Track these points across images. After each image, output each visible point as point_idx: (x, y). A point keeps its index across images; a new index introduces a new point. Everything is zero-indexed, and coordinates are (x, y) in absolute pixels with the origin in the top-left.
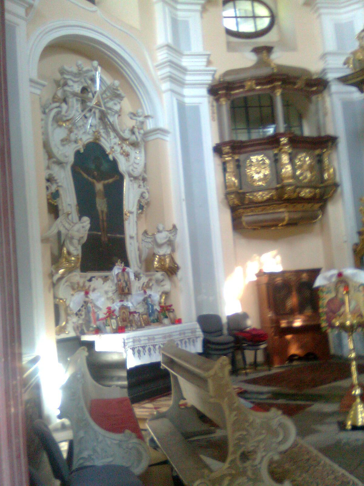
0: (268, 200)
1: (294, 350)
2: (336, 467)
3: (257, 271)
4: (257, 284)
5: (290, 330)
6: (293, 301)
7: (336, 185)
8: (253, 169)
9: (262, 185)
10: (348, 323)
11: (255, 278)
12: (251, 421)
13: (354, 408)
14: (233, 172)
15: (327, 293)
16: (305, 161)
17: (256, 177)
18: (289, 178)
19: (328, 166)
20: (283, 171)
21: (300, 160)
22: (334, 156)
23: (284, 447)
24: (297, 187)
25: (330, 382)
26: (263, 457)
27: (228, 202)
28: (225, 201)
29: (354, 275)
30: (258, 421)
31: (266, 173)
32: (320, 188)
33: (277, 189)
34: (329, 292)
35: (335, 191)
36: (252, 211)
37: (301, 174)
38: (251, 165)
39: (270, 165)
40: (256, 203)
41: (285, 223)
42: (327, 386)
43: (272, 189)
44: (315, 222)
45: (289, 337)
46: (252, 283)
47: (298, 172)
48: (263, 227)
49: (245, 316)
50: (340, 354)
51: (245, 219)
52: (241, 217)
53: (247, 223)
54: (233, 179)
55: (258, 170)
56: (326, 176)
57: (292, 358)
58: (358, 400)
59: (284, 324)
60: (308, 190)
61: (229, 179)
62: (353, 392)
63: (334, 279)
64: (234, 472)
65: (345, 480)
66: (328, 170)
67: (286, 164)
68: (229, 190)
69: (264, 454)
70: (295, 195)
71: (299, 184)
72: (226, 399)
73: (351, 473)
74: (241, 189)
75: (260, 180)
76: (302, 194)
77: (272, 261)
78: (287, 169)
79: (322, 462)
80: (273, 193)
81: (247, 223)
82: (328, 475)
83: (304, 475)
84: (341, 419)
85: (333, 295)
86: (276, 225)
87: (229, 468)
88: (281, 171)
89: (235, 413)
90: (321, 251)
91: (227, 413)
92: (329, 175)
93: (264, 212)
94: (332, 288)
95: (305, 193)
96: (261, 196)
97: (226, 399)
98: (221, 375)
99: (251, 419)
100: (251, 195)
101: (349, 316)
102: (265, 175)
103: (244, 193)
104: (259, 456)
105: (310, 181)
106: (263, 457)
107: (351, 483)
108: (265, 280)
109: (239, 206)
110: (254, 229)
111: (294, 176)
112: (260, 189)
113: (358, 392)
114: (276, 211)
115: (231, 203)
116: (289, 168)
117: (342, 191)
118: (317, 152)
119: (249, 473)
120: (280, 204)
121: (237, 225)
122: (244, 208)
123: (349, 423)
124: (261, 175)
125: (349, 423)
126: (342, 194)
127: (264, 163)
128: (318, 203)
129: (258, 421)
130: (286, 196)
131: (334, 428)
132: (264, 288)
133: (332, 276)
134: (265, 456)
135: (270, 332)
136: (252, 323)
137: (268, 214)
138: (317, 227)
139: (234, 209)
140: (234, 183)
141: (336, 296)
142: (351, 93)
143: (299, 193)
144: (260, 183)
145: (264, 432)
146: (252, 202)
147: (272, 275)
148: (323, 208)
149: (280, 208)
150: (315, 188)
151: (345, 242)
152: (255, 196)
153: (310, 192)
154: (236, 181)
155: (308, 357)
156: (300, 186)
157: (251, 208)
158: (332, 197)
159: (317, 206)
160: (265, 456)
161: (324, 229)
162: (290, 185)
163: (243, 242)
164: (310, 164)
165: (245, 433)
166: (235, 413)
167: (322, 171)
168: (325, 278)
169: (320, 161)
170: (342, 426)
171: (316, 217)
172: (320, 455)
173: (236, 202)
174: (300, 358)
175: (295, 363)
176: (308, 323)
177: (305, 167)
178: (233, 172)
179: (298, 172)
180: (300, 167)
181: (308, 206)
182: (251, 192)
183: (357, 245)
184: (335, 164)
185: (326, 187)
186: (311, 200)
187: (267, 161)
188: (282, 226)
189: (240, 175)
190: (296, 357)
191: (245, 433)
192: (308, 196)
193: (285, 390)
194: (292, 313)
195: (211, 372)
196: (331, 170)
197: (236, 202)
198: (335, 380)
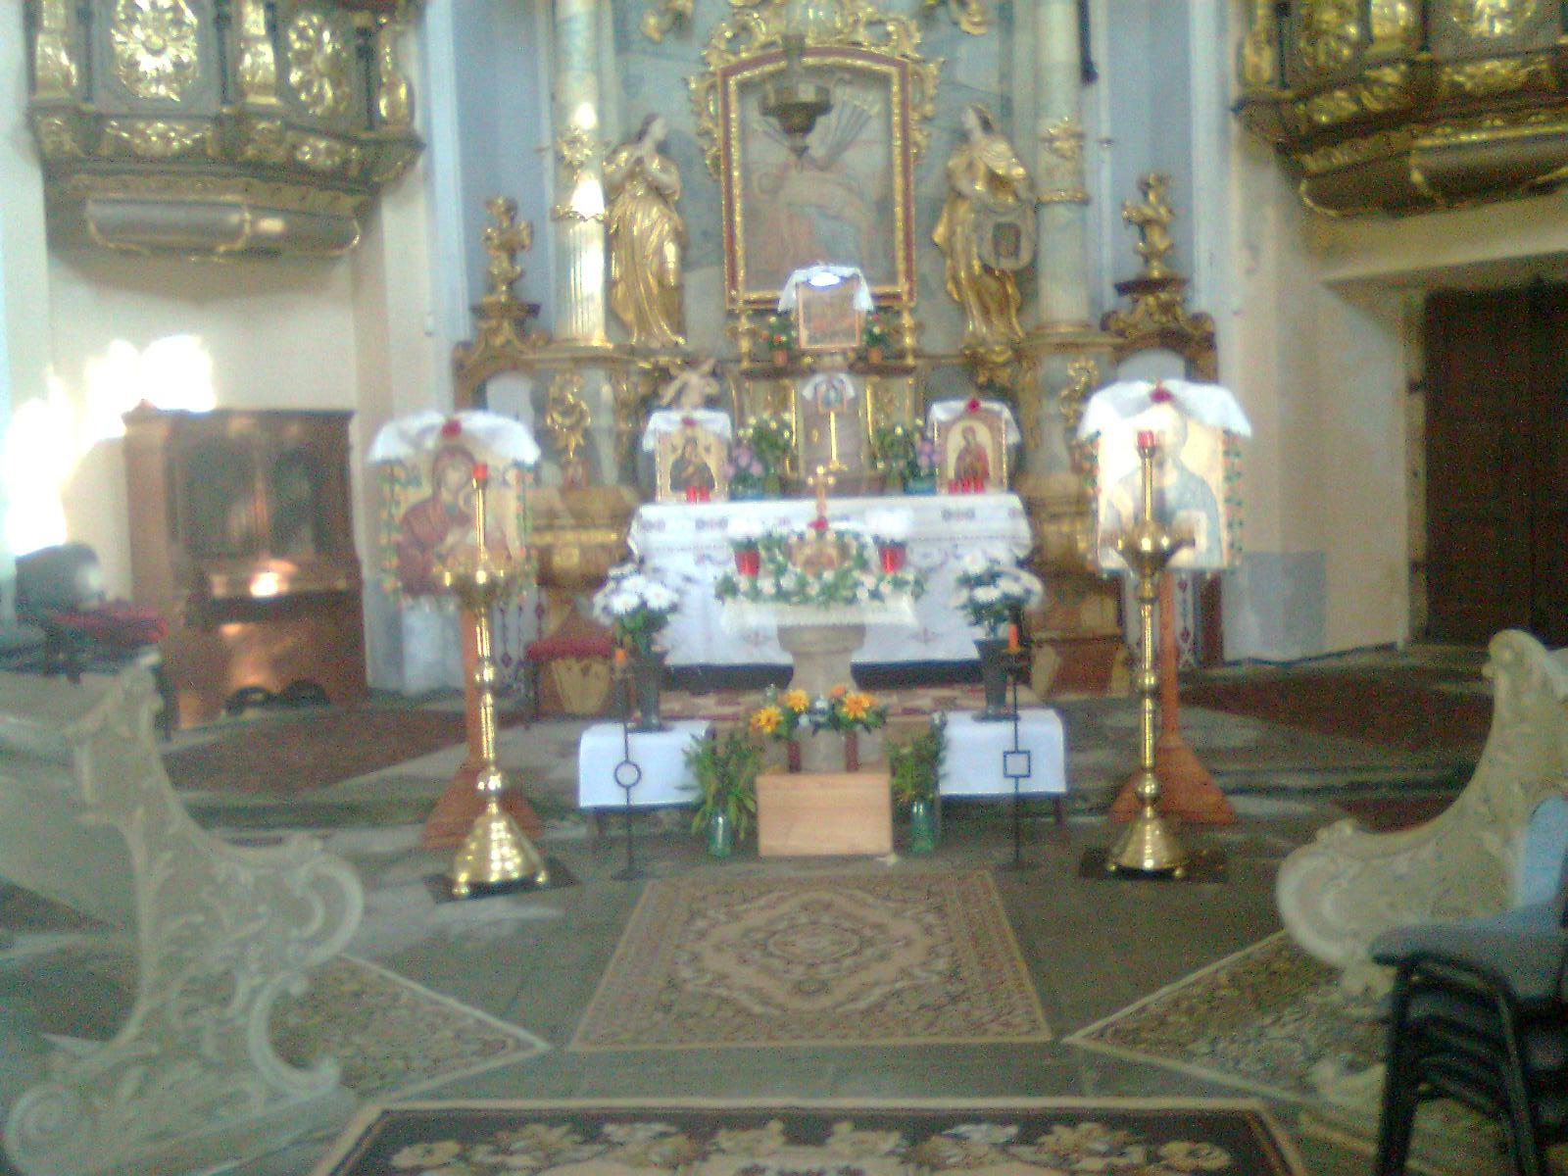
0: (184, 155)
1: (250, 674)
2: (451, 1002)
3: (131, 406)
4: (132, 452)
5: (245, 608)
6: (251, 513)
7: (415, 144)
8: (138, 32)
9: (166, 99)
10: (481, 578)
11: (120, 431)
12: (220, 879)
13: (479, 832)
14: (64, 33)
15: (405, 486)
16: (319, 42)
17: (148, 64)
18: (263, 88)
19: (1527, 55)
20: (248, 60)
21: (302, 35)
22: (411, 46)
23: (320, 955)
24: (289, 126)
25: (379, 767)
26: (255, 992)
27: (37, 142)
28: (26, 137)
29: (493, 434)
30: (246, 877)
31: (185, 59)
32: (362, 144)
33: (218, 120)
34: (414, 481)
35: (409, 164)
36: (126, 187)
37: (305, 85)
38: (131, 20)
39: (200, 34)
40: (153, 160)
41: (239, 245)
42: (373, 777)
43: (204, 118)
44: (339, 257)
45: (232, 630)
46: (110, 444)
47: (295, 77)
48: (159, 250)
49: (81, 554)
50: (391, 684)
51: (95, 212)
52: (81, 203)
53: (102, 229)
54: (64, 59)
55: (157, 41)
56: (383, 105)
57: (242, 699)
58: (493, 808)
59: (219, 587)
60: (322, 145)
61: (45, 57)
62: (481, 786)
63: (430, 443)
64: (155, 1050)
65: (490, 1038)
66: (392, 88)
67: (257, 39)
68: (44, 95)
69: (258, 980)
70: (278, 155)
71: (294, 119)
72: (140, 812)
73: (502, 1015)
74: (88, 99)
75: (159, 79)
76: (306, 155)
77: (181, 366)
78: (260, 59)
79: (405, 997)
80: (206, 132)
81: (102, 229)
82: (433, 1028)
83: (357, 1039)
84: (431, 867)
85: (426, 491)
86: (207, 251)
87: (139, 1038)
88: (240, 58)
89: (168, 855)
90: (368, 350)
91: (139, 858)
92: (393, 106)
93: (167, 196)
94: (424, 468)
95: (313, 151)
96: (163, 136)
97: (140, 812)
98: (124, 731)
99: (222, 870)
100: (122, 128)
101: (484, 556)
102: (179, 65)
103: (100, 118)
104: (243, 987)
105: (333, 112)
106: (255, 992)
107: (510, 1042)
108: (158, 434)
109: (76, 159)
110: (126, 253)
111: (281, 86)
112: (160, 110)
113: (495, 782)
114: (212, 197)
115: (48, 146)
116: (267, 54)
117: (430, 162)
118: (360, 19)
119: (209, 1049)
120: (227, 176)
121: (68, 234)
122: (92, 172)
123: (463, 877)
124: (165, 63)
125: (463, 877)
126: (428, 175)
127: (178, 22)
128: (350, 192)
129: (246, 877)
130: (250, 152)
131: (419, 895)
132: (155, 465)
133: (425, 432)
134: (263, 985)
135: (177, 608)
136: (104, 580)
137: (182, 203)
138: (342, 273)
139: (54, 170)
140: (67, 76)
141: (435, 497)
142: (1368, 99)
143: (295, 147)
144: (162, 90)
145: (262, 909)
146: (125, 151)
147: (180, 421)
148: (367, 215)
149: (226, 190)
150: (349, 140)
151: (429, 334)
152: (142, 134)
153: (330, 152)
154: (73, 69)
155: (296, 693)
156: (298, 124)
157: (118, 173)
158: (398, 179)
159: (348, 203)
160: (263, 985)
161: (365, 285)
162: (266, 113)
163: (81, 294)
164: (336, 53)
165: (199, 918)
166: (168, 855)
167: (370, 86)
168: (403, 436)
169: (365, 51)
170: (443, 888)
171: (342, 241)
172: (391, 975)
173: (69, 144)
174: (269, 700)
175: (251, 715)
176: (313, 586)
177: (319, 61)
178: (64, 33)
179: (295, 77)
180: (303, 58)
181: (319, 199)
182: (126, 117)
183: (465, 346)
184: (413, 71)
185: (379, 144)
186: (333, 179)
187: (190, 17)
188: (229, 254)
189: (88, 44)
190: (259, 697)
191: (199, 918)
192: (325, 163)
193: (234, 799)
194: (250, 552)
195: (89, 724)
196: (403, 92)
197: (69, 144)
198: (393, 759)
